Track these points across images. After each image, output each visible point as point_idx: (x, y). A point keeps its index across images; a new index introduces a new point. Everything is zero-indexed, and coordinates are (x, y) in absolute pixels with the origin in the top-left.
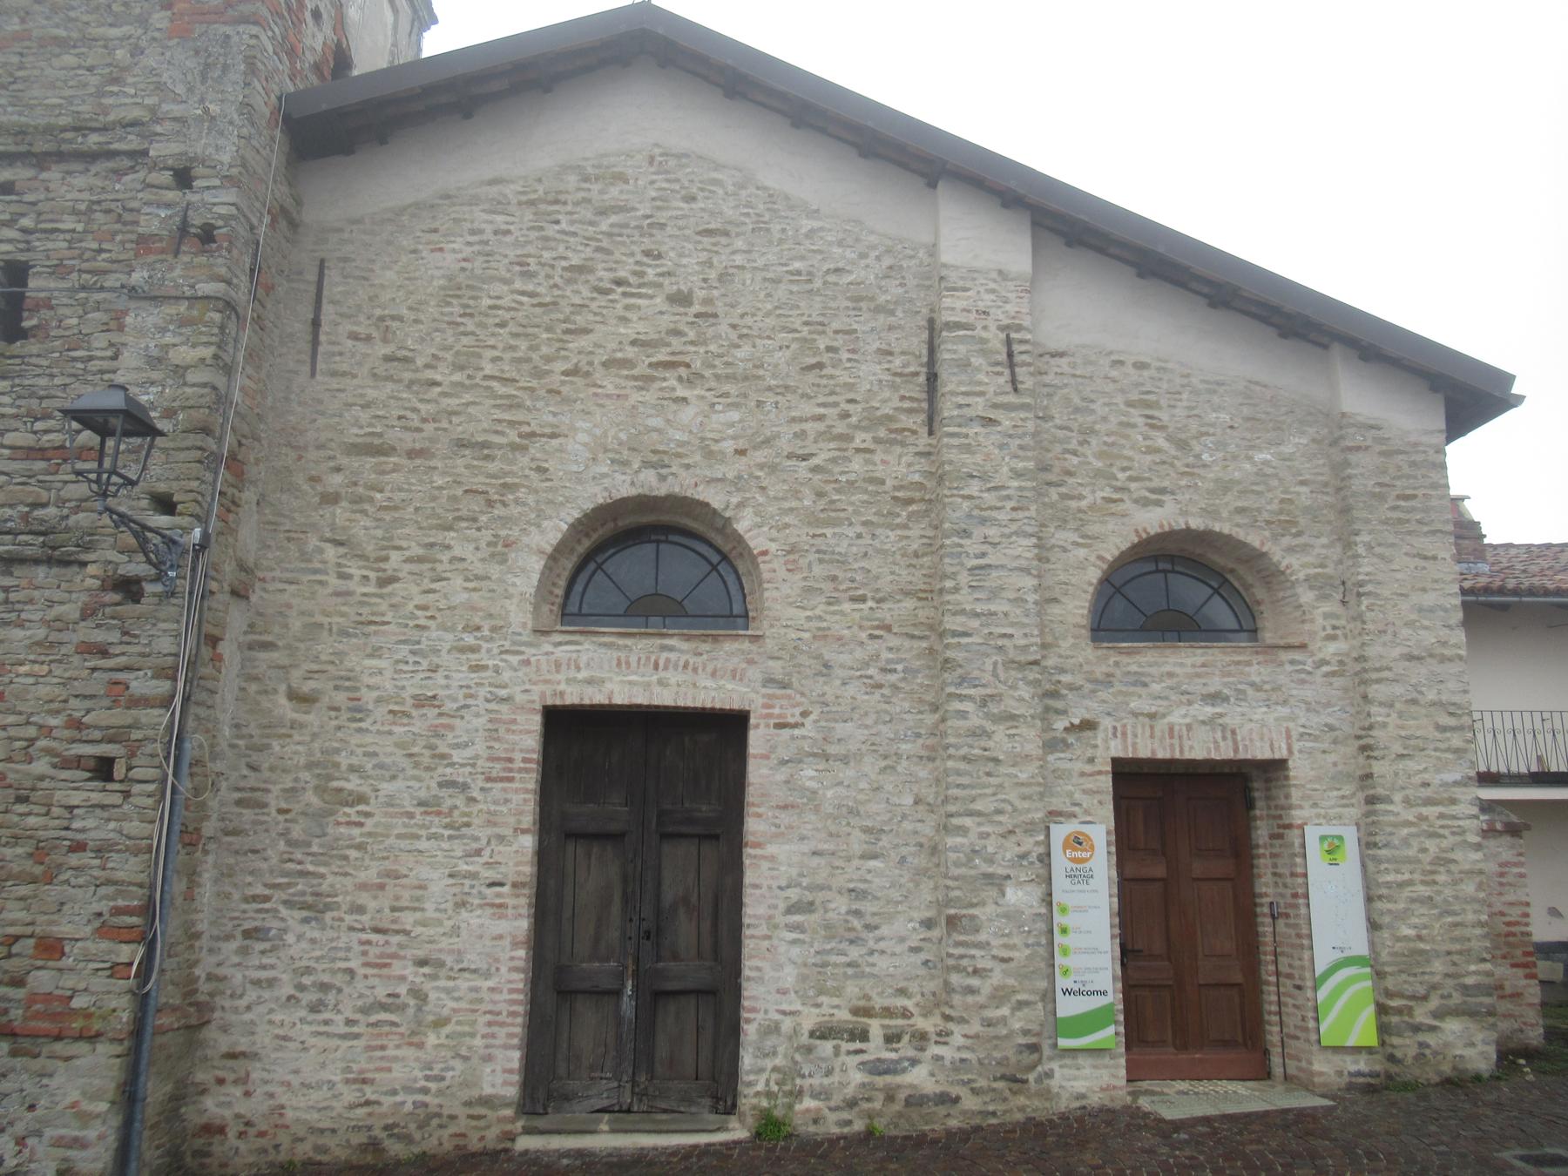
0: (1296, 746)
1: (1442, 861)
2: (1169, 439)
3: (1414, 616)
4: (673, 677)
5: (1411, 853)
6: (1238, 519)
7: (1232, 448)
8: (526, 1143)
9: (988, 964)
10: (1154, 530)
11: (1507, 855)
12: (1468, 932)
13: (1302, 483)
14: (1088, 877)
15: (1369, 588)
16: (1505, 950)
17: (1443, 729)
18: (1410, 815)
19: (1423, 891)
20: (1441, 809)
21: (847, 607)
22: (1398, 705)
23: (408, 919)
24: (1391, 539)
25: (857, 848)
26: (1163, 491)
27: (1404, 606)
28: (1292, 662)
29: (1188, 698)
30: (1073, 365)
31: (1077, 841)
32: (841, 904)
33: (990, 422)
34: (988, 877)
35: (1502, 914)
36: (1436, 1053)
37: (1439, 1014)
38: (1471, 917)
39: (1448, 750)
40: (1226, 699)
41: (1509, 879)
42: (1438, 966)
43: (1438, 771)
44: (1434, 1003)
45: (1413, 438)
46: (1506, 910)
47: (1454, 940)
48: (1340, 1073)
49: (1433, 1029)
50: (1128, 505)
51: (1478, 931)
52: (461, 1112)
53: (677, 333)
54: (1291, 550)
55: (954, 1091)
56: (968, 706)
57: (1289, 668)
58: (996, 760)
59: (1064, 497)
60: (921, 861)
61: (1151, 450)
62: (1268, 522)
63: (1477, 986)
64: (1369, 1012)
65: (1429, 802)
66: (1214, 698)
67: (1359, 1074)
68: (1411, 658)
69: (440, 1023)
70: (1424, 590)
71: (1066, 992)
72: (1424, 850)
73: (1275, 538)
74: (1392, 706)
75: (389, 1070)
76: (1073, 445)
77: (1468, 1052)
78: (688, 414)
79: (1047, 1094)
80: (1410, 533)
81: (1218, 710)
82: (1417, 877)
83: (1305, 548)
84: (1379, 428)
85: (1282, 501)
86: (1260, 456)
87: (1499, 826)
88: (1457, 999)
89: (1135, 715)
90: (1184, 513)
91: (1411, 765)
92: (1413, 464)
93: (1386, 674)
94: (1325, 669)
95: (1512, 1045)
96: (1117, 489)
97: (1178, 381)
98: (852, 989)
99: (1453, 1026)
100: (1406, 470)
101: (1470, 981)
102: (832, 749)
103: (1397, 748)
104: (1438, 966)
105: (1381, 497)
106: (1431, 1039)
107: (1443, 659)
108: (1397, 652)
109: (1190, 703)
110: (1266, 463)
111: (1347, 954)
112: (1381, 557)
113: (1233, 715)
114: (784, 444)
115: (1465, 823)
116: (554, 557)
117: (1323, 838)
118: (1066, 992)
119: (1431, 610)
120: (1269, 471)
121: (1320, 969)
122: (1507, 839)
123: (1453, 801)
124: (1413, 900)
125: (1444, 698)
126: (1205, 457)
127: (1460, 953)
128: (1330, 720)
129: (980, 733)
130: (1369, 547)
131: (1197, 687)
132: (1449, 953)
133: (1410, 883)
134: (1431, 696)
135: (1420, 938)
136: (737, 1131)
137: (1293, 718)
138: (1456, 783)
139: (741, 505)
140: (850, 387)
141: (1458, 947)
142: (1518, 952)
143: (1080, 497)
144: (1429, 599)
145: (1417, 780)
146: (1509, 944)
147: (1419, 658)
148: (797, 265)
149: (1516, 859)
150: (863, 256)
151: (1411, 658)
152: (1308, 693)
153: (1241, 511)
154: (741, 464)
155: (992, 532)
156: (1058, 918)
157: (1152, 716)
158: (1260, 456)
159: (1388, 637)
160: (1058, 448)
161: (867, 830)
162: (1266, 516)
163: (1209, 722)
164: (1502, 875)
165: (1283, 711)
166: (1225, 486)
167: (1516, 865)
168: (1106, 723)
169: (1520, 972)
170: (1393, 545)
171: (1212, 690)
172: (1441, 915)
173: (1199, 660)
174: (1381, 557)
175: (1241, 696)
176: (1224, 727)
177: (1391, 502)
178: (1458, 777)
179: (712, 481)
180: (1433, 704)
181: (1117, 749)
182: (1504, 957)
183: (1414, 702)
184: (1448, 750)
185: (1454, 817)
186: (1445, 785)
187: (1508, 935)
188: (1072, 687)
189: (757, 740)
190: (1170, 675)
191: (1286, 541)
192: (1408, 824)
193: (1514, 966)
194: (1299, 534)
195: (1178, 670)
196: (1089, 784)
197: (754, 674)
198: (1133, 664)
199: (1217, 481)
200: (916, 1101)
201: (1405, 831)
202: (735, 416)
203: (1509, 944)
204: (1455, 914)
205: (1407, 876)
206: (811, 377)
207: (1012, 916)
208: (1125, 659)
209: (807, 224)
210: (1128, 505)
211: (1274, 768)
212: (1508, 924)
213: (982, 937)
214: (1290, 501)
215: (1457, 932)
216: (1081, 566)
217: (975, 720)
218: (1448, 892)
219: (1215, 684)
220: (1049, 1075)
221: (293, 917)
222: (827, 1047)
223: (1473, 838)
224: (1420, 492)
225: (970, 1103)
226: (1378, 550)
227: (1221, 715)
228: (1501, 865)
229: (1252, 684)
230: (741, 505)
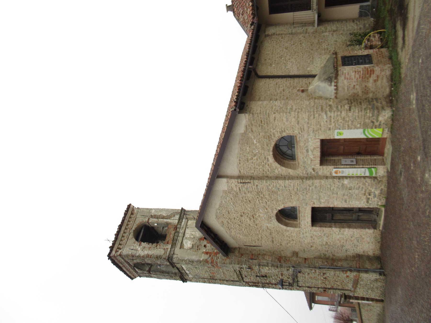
0: (318, 138)
1: (344, 119)
2: (254, 157)
3: (289, 122)
4: (306, 215)
5: (341, 124)
6: (269, 146)
7: (254, 147)
8: (381, 228)
9: (358, 186)
10: (273, 160)
11: (343, 78)
12: (360, 115)
13: (260, 134)
14: (343, 171)
15: (283, 129)
16: (366, 79)
17: (314, 118)
18: (333, 124)
19: (350, 123)
20: (332, 119)
21: (292, 197)
22: (309, 125)
23: (345, 238)
24: (271, 125)
25: (336, 195)
26: (265, 158)
27: (286, 123)
28: (299, 138)
29: (307, 155)
30: (242, 170)
31: (336, 172)
32: (346, 197)
33: (257, 186)
34: (342, 186)
35: (357, 79)
36: (386, 122)
37: (377, 120)
38: (357, 114)
39: (319, 117)
40: (308, 149)
41: (349, 77)
42: (367, 121)
43: (324, 119)
44: (375, 121)
45: (247, 120)
46: (356, 78)
47: (361, 118)
48: (387, 133)
49: (380, 122)
50: (269, 163)
51: (360, 113)
52: (375, 234)
53: (247, 216)
54: (274, 136)
55: (380, 189)
56: (311, 188)
57: (300, 139)
58: (320, 185)
59: (268, 171)
60: (326, 42)
61: (257, 159)
62: (269, 141)
63: (372, 114)
64: (376, 130)
65: (330, 121)
66: (307, 151)
67: (388, 130)
68: (298, 123)
69: (361, 236)
70: (282, 120)
71: (365, 174)
72: (341, 122)
73: (272, 139)
74: (309, 127)
75: (368, 74)
76: (258, 170)
77: (387, 116)
78: (261, 215)
79: (383, 177)
80: (269, 121)
81: (310, 150)
82: (347, 123)
83: (274, 134)
84: (246, 126)
85: (264, 138)
86: (255, 142)
87: (335, 81)
88: (374, 117)
89: (311, 163)
90: (269, 155)
91: (322, 124)
92: (254, 120)
93: (302, 128)
94: (300, 132)
95: (390, 79)
96: (266, 164)
97: (241, 155)
98: (361, 195)
99: (380, 119)
100: (255, 121)
101: (371, 115)
102: (318, 198)
103: (318, 126)
104: (367, 121)
105: (262, 126)
106: (383, 122)
107: (298, 117)
108: (297, 126)
109: (309, 155)
110: (256, 141)
111: (362, 132)
112: (276, 127)
113: (311, 148)
114: (265, 205)
115: (336, 115)
116: (286, 225)
117: (337, 135)
118: (365, 174)
119: (287, 119)
120: (258, 141)
121: (365, 137)
122: (339, 77)
123: (330, 117)
124: (352, 125)
125: (307, 117)
126: (257, 152)
127: (364, 117)
128: (312, 132)
129: (316, 187)
130: (274, 129)
131: (305, 154)
132: (364, 119)
133: (348, 125)
134: (307, 120)
135: (360, 124)
136: (383, 209)
137: (311, 138)
138: (326, 116)
139: (276, 209)
140: (252, 197)
141: (363, 117)
142: (367, 76)
143: (268, 169)
144: (285, 119)
145: (325, 123)
146: (365, 78)
147: (298, 122)
148: (232, 204)
149: (344, 76)
150: (228, 196)
151: (298, 123)
152: (306, 136)
153: (267, 145)
154: (269, 209)
155: (278, 185)
156: (351, 175)
157: (311, 160)
158: (255, 142)
159: (294, 127)
160: (259, 172)
161: (333, 194)
162: (268, 141)
163: (312, 151)
164: (347, 79)
165: (310, 140)
166: (263, 148)
167: (345, 75)
168: (313, 167)
169: (372, 75)
170: (273, 125)
171: (306, 152)
172: (356, 120)
173: (300, 153)
174: (276, 127)
175: (307, 147)
176: (313, 149)
177: (263, 124)
178: (325, 116)
179: (272, 212)
180: (308, 120)
181: (318, 165)
182: (368, 79)
183: (308, 123)
184: (319, 117)
185: (334, 116)
186: (327, 118)
187: (362, 78)
188: (306, 171)
189: (316, 205)
190: (303, 158)
191: (273, 137)
192: (335, 125)
193: (370, 76)
194: (271, 135)
195: (302, 157)
196: (325, 169)
197: (305, 207)
198: (301, 163)
199: (262, 150)
200: (381, 193)
201: (337, 125)
202: (260, 210)
203: (365, 78)
204: (356, 117)
205: (347, 126)
206: (252, 202)
207: (349, 183)
208: (300, 164)
209: (223, 202)
210: (269, 163)
211: (322, 141)
212: (360, 78)
213: (353, 186)
214: (264, 136)
215: (360, 117)
216: (282, 170)
217: (313, 187)
218: (351, 118)
219: (305, 151)
220: (379, 176)
221: (344, 248)
222: (370, 202)
223: (339, 113)
224: (260, 119)
225: (383, 187)
226: (274, 128)
227: (311, 150)
228: (345, 79)
229: (304, 145)
230: (276, 209)
